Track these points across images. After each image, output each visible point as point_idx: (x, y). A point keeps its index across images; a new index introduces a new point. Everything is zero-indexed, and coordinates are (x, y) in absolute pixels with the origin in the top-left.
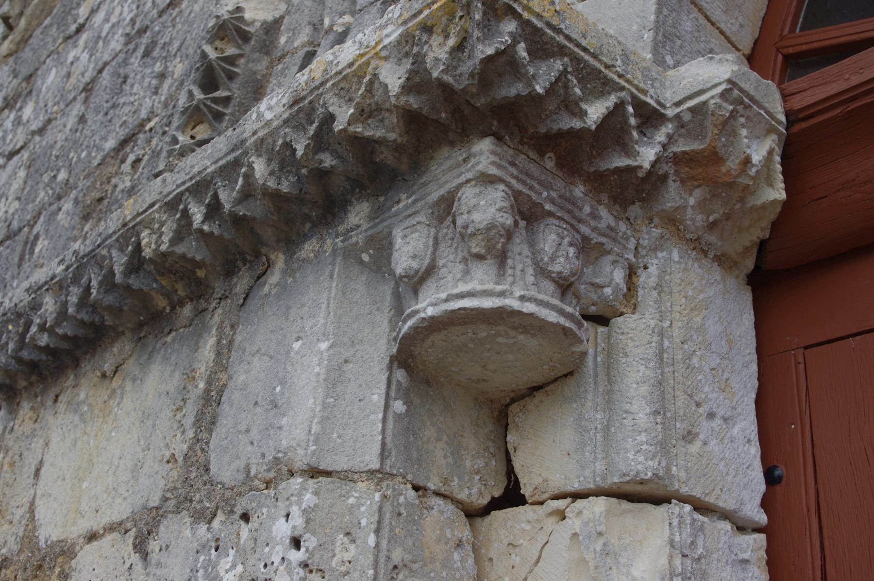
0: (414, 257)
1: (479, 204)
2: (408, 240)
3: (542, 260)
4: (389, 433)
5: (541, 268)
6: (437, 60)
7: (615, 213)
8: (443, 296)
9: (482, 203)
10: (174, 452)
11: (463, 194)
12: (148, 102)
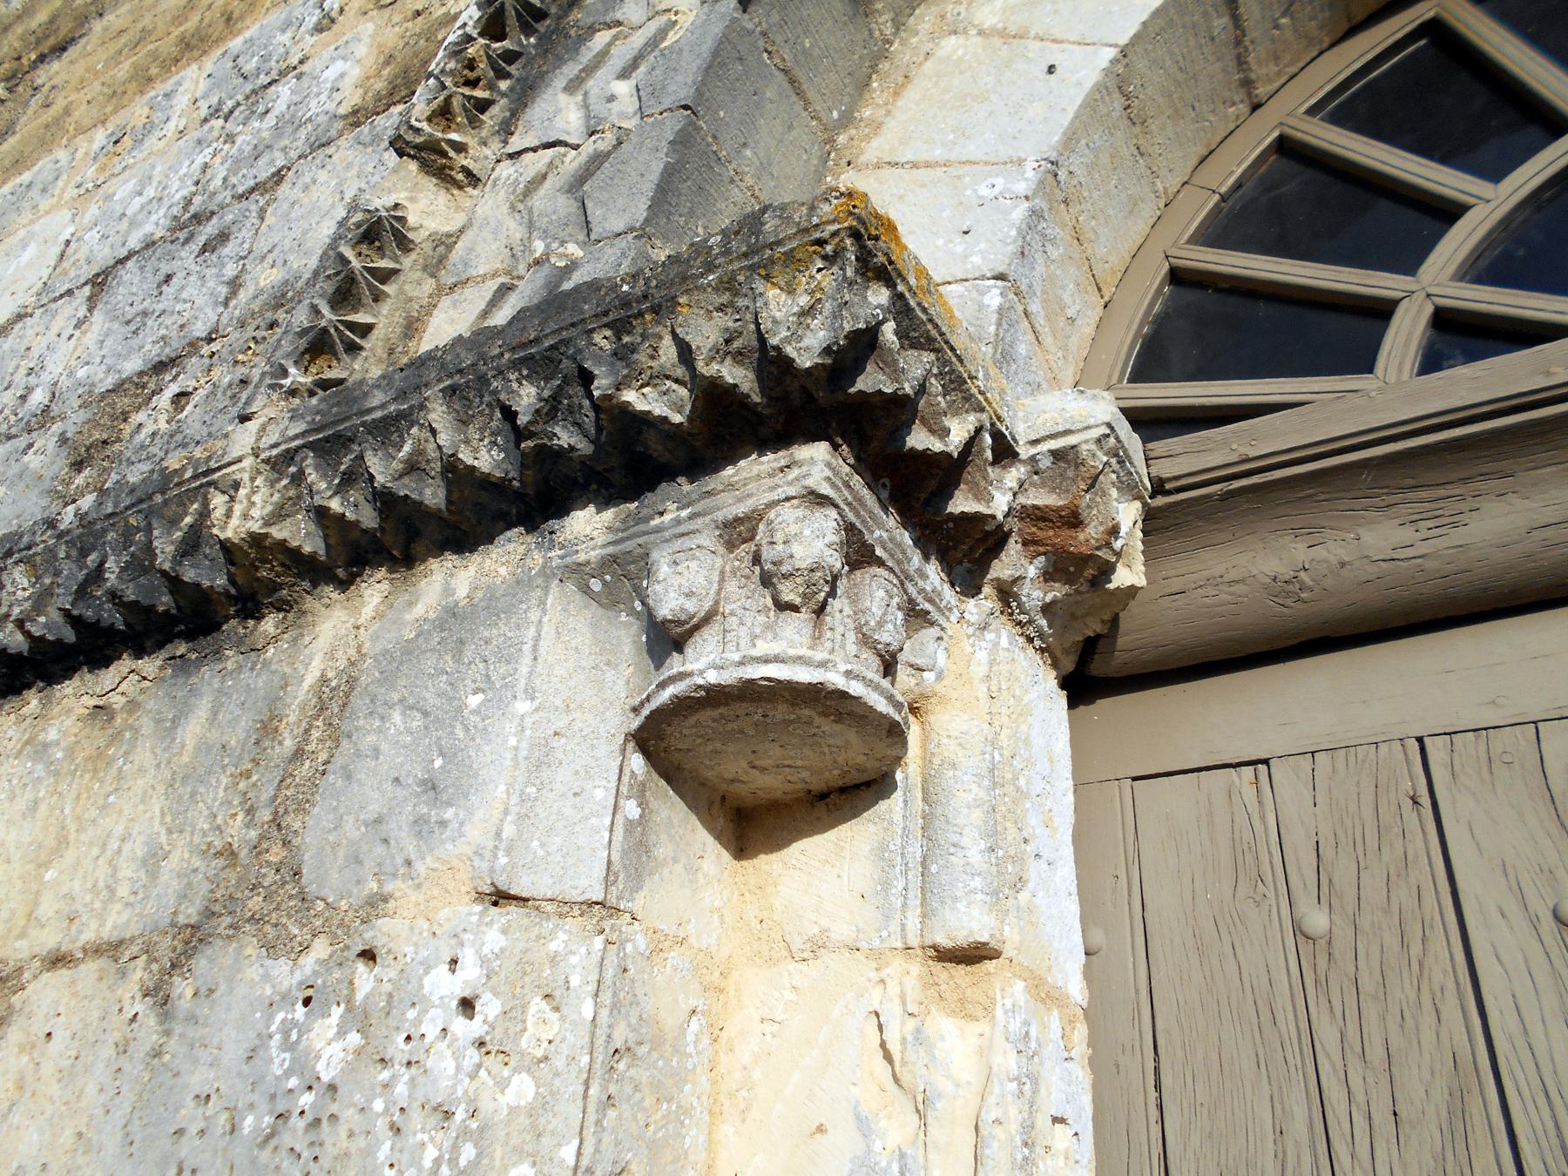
0: (689, 595)
2: (679, 569)
3: (867, 623)
4: (616, 845)
5: (864, 635)
9: (807, 532)
10: (230, 840)
12: (211, 315)
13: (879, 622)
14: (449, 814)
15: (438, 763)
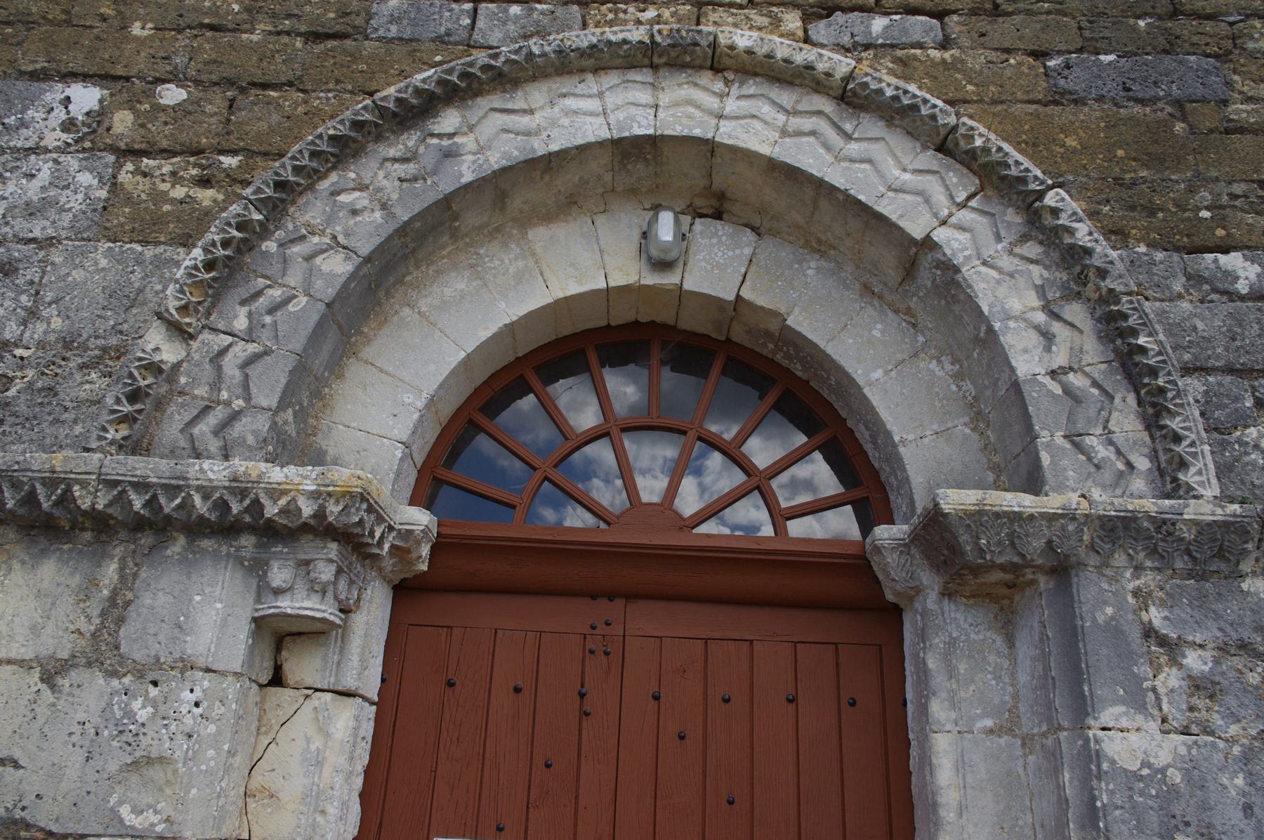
6: (332, 512)
14: (188, 639)
15: (182, 618)
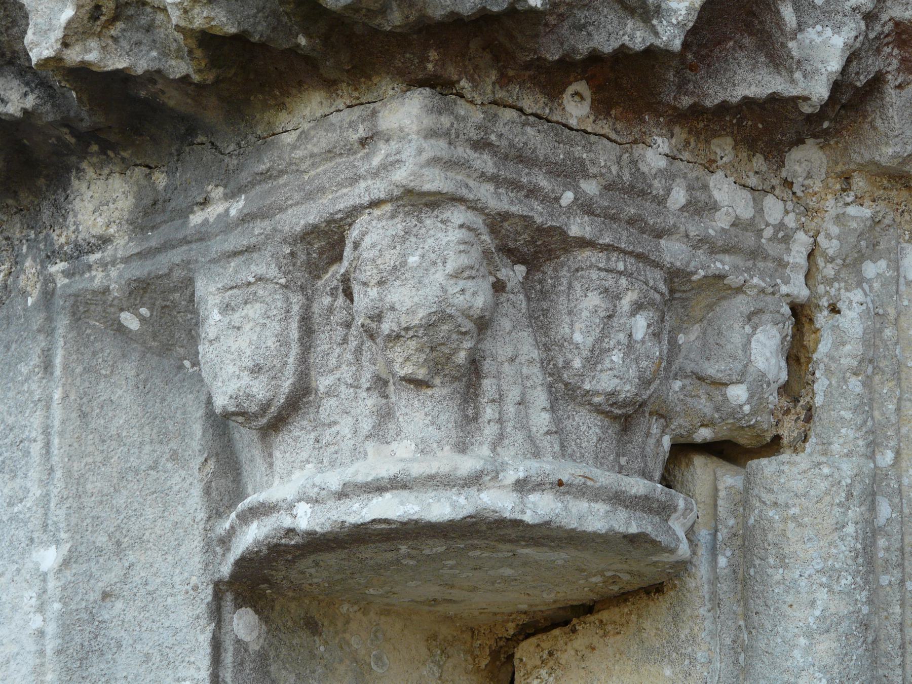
0: (256, 370)
1: (404, 264)
2: (236, 317)
3: (567, 364)
7: (753, 181)
8: (334, 480)
9: (413, 260)
11: (363, 234)
13: (587, 360)
